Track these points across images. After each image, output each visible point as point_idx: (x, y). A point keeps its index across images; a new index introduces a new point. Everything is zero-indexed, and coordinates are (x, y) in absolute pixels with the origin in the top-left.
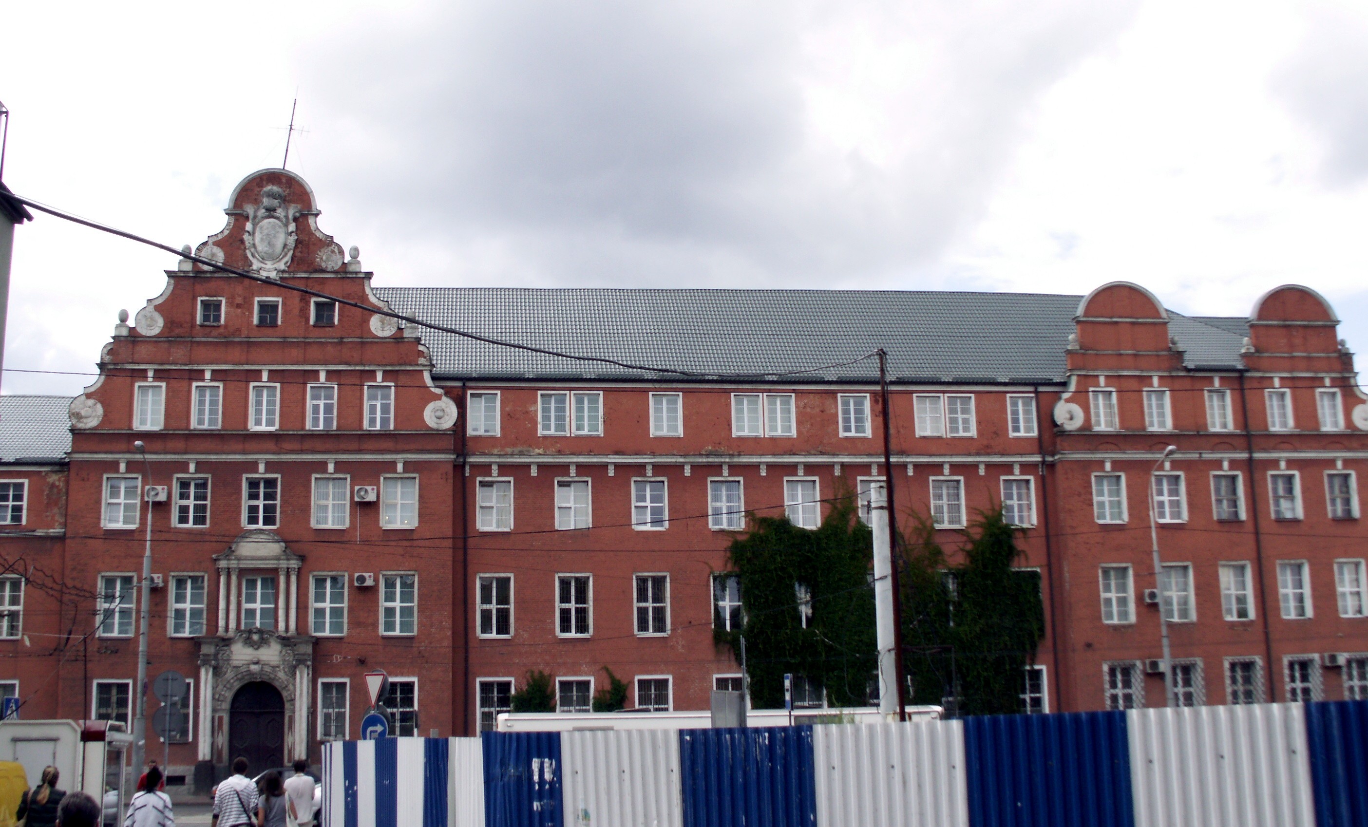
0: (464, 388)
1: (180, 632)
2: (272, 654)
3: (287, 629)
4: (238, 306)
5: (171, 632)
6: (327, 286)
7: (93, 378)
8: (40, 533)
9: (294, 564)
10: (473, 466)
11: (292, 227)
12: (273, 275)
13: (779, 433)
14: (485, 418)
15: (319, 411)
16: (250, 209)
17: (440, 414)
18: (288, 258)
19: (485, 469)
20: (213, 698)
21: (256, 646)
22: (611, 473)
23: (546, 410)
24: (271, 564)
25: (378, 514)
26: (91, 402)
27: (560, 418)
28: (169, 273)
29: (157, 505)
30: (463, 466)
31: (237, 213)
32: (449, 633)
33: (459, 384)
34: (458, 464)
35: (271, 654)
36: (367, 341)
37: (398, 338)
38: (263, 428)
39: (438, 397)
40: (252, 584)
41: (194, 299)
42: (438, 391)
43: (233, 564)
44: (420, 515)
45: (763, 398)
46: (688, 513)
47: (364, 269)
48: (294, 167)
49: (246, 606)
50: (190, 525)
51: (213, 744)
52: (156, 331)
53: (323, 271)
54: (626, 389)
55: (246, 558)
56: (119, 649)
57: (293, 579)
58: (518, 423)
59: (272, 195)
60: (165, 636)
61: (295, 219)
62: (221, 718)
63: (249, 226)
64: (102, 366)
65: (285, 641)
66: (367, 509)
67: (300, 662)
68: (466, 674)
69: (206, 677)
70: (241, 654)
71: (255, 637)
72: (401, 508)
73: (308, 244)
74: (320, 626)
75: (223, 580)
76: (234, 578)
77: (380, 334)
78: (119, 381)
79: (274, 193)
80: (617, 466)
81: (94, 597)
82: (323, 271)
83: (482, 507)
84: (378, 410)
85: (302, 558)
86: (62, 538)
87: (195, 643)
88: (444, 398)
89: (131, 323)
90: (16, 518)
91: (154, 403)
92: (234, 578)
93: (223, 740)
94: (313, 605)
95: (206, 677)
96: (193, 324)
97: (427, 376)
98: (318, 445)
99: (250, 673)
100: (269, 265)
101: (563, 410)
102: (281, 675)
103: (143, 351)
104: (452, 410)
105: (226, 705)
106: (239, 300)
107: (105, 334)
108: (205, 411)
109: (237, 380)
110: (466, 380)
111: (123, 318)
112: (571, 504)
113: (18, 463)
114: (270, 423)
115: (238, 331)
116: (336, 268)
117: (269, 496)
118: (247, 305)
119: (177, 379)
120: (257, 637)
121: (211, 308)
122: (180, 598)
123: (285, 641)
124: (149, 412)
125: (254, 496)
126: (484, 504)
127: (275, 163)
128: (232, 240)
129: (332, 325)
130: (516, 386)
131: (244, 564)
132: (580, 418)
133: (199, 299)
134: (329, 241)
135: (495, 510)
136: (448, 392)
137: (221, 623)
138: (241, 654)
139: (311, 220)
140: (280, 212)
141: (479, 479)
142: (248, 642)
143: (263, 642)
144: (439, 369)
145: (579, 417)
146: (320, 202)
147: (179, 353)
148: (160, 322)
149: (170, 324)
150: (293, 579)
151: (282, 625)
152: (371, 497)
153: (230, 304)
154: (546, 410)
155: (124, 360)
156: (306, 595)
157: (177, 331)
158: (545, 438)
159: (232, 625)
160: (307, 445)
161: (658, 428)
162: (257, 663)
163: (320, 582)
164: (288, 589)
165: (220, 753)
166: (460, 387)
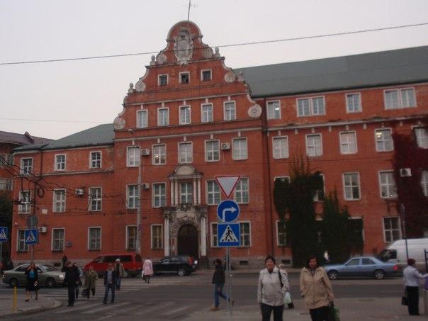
0: (265, 101)
1: (341, 262)
2: (191, 214)
3: (174, 204)
4: (174, 76)
5: (153, 205)
6: (207, 61)
7: (121, 109)
8: (106, 170)
9: (199, 177)
10: (271, 132)
11: (192, 43)
12: (185, 63)
13: (408, 106)
14: (275, 111)
15: (206, 115)
16: (175, 38)
17: (255, 111)
18: (191, 55)
19: (275, 133)
20: (170, 232)
21: (185, 210)
22: (330, 130)
23: (300, 106)
24: (190, 177)
25: (231, 155)
26: (121, 119)
27: (307, 109)
28: (147, 67)
29: (147, 156)
30: (266, 132)
31: (171, 40)
32: (263, 202)
33: (263, 99)
34: (264, 131)
35: (191, 214)
36: (224, 84)
37: (236, 82)
38: (185, 123)
39: (254, 104)
40: (183, 185)
41: (157, 76)
42: (253, 102)
43: (176, 178)
44: (249, 153)
45: (399, 91)
46: (365, 143)
47: (222, 56)
48: (192, 20)
49: (182, 194)
50: (160, 164)
51: (170, 250)
52: (143, 90)
53: (205, 59)
54: (335, 93)
55: (181, 175)
56: (133, 212)
57: (199, 183)
58: (288, 111)
59: (183, 31)
60: (151, 207)
61: (193, 40)
62: (173, 240)
63: (175, 45)
64: (124, 105)
65: (197, 208)
66: (227, 152)
67: (202, 216)
68: (272, 219)
69: (167, 223)
70: (180, 214)
71: (185, 206)
72: (240, 151)
73: (200, 49)
74: (210, 201)
75: (172, 184)
76: (176, 184)
77: (229, 81)
78: (131, 109)
79: (185, 32)
80: (332, 127)
81: (142, 199)
82: (205, 59)
83: (343, 145)
84: (230, 114)
85: (202, 174)
86: (113, 172)
87: (162, 209)
88: (256, 105)
89: (134, 88)
90: (99, 166)
91: (144, 117)
92: (176, 184)
93: (174, 248)
94: (207, 193)
95: (167, 223)
96: (157, 86)
97: (248, 96)
98: (232, 126)
99: (184, 221)
100: (184, 59)
101: (308, 105)
102: (196, 221)
103: (140, 97)
104: (260, 109)
105: (176, 234)
106: (173, 74)
107: (124, 93)
108: (163, 119)
109: (174, 106)
110: (266, 97)
111: (131, 86)
112: (348, 142)
113: (98, 145)
114: (188, 121)
115: (174, 86)
116: (210, 57)
117: (30, 164)
118: (177, 76)
119: (152, 106)
120: (185, 207)
121: (163, 78)
122: (157, 193)
123: (197, 208)
124: (142, 121)
125: (94, 159)
126: (344, 143)
127: (185, 19)
128: (169, 52)
129: (210, 80)
130: (288, 96)
131: (179, 178)
132: (315, 108)
133: (159, 76)
134: (207, 47)
135: (384, 143)
136: (258, 102)
137: (172, 203)
138: (180, 214)
139: (199, 39)
140: (187, 38)
141: (273, 137)
142: (182, 209)
143: (188, 208)
144: (253, 94)
145: (311, 108)
146: (203, 31)
147: (153, 96)
148: (145, 86)
149: (148, 86)
150: (199, 183)
151: (195, 202)
152: (228, 147)
153: (170, 76)
154: (300, 106)
155: (132, 101)
156: (204, 189)
157: (151, 89)
158: (300, 118)
159: (176, 203)
160: (227, 126)
161: (351, 109)
162: (186, 216)
163: (210, 183)
164: (197, 187)
165: (174, 253)
166: (263, 100)
